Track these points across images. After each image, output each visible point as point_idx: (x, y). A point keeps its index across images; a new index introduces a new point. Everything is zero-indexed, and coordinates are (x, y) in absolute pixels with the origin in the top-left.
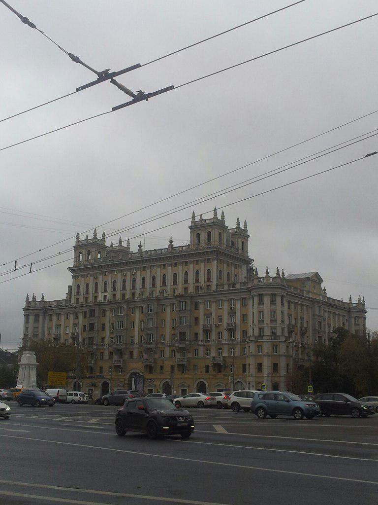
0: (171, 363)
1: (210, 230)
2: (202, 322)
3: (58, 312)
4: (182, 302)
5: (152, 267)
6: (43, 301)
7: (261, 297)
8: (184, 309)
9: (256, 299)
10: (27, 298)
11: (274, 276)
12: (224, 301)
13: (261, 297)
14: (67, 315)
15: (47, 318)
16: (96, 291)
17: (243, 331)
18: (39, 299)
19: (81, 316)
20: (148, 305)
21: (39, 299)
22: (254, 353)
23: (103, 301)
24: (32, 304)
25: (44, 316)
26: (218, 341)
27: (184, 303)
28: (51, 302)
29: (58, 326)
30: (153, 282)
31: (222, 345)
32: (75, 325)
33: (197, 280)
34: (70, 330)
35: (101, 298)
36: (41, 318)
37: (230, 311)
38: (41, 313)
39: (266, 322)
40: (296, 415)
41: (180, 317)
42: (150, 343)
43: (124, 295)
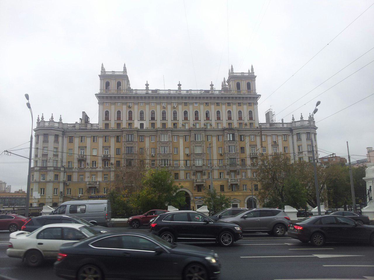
0: (220, 183)
1: (239, 81)
2: (248, 151)
3: (82, 134)
4: (230, 134)
5: (162, 103)
6: (60, 123)
7: (298, 134)
8: (231, 139)
9: (295, 137)
10: (38, 118)
11: (58, 122)
12: (99, 137)
13: (298, 134)
14: (94, 139)
15: (66, 140)
16: (130, 118)
17: (93, 162)
18: (57, 120)
19: (113, 141)
20: (195, 134)
21: (57, 120)
22: (38, 180)
23: (139, 128)
24: (41, 125)
25: (63, 137)
26: (104, 168)
27: (231, 135)
28: (69, 124)
29: (82, 148)
30: (129, 115)
31: (73, 172)
32: (106, 148)
33: (240, 118)
34: (101, 153)
35: (137, 124)
36: (60, 139)
37: (273, 144)
38: (60, 133)
39: (49, 156)
40: (10, 229)
41: (229, 146)
42: (95, 168)
43: (119, 125)
